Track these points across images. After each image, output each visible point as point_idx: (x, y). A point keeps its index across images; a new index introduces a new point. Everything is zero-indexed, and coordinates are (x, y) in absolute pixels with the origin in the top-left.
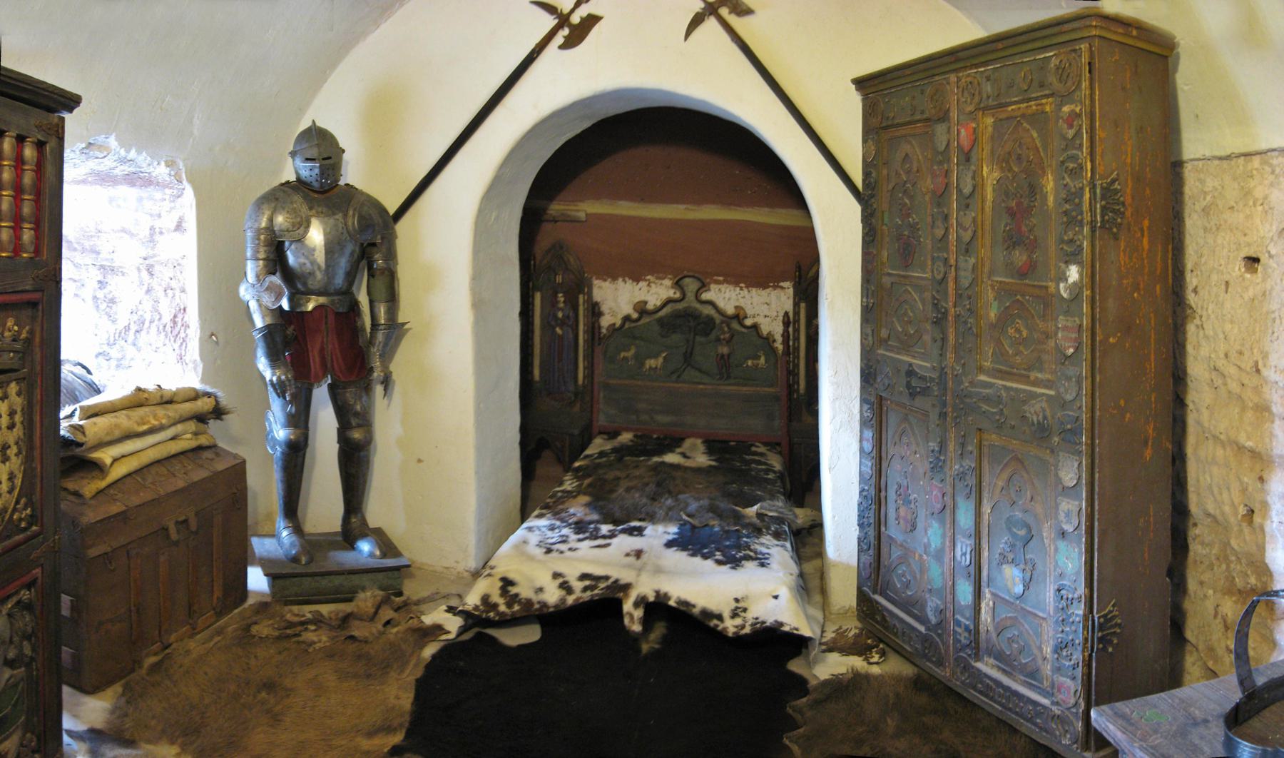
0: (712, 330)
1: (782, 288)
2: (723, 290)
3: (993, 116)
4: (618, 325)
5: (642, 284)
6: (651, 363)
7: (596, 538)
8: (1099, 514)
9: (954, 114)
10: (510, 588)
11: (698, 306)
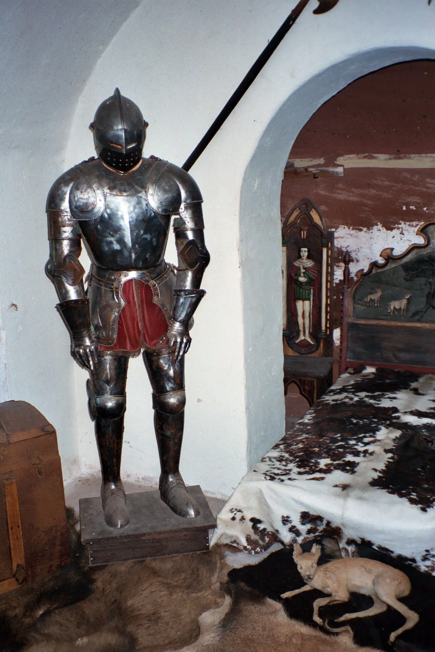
4: (365, 271)
5: (396, 232)
6: (395, 305)
7: (314, 472)
8: (314, 385)
10: (259, 525)
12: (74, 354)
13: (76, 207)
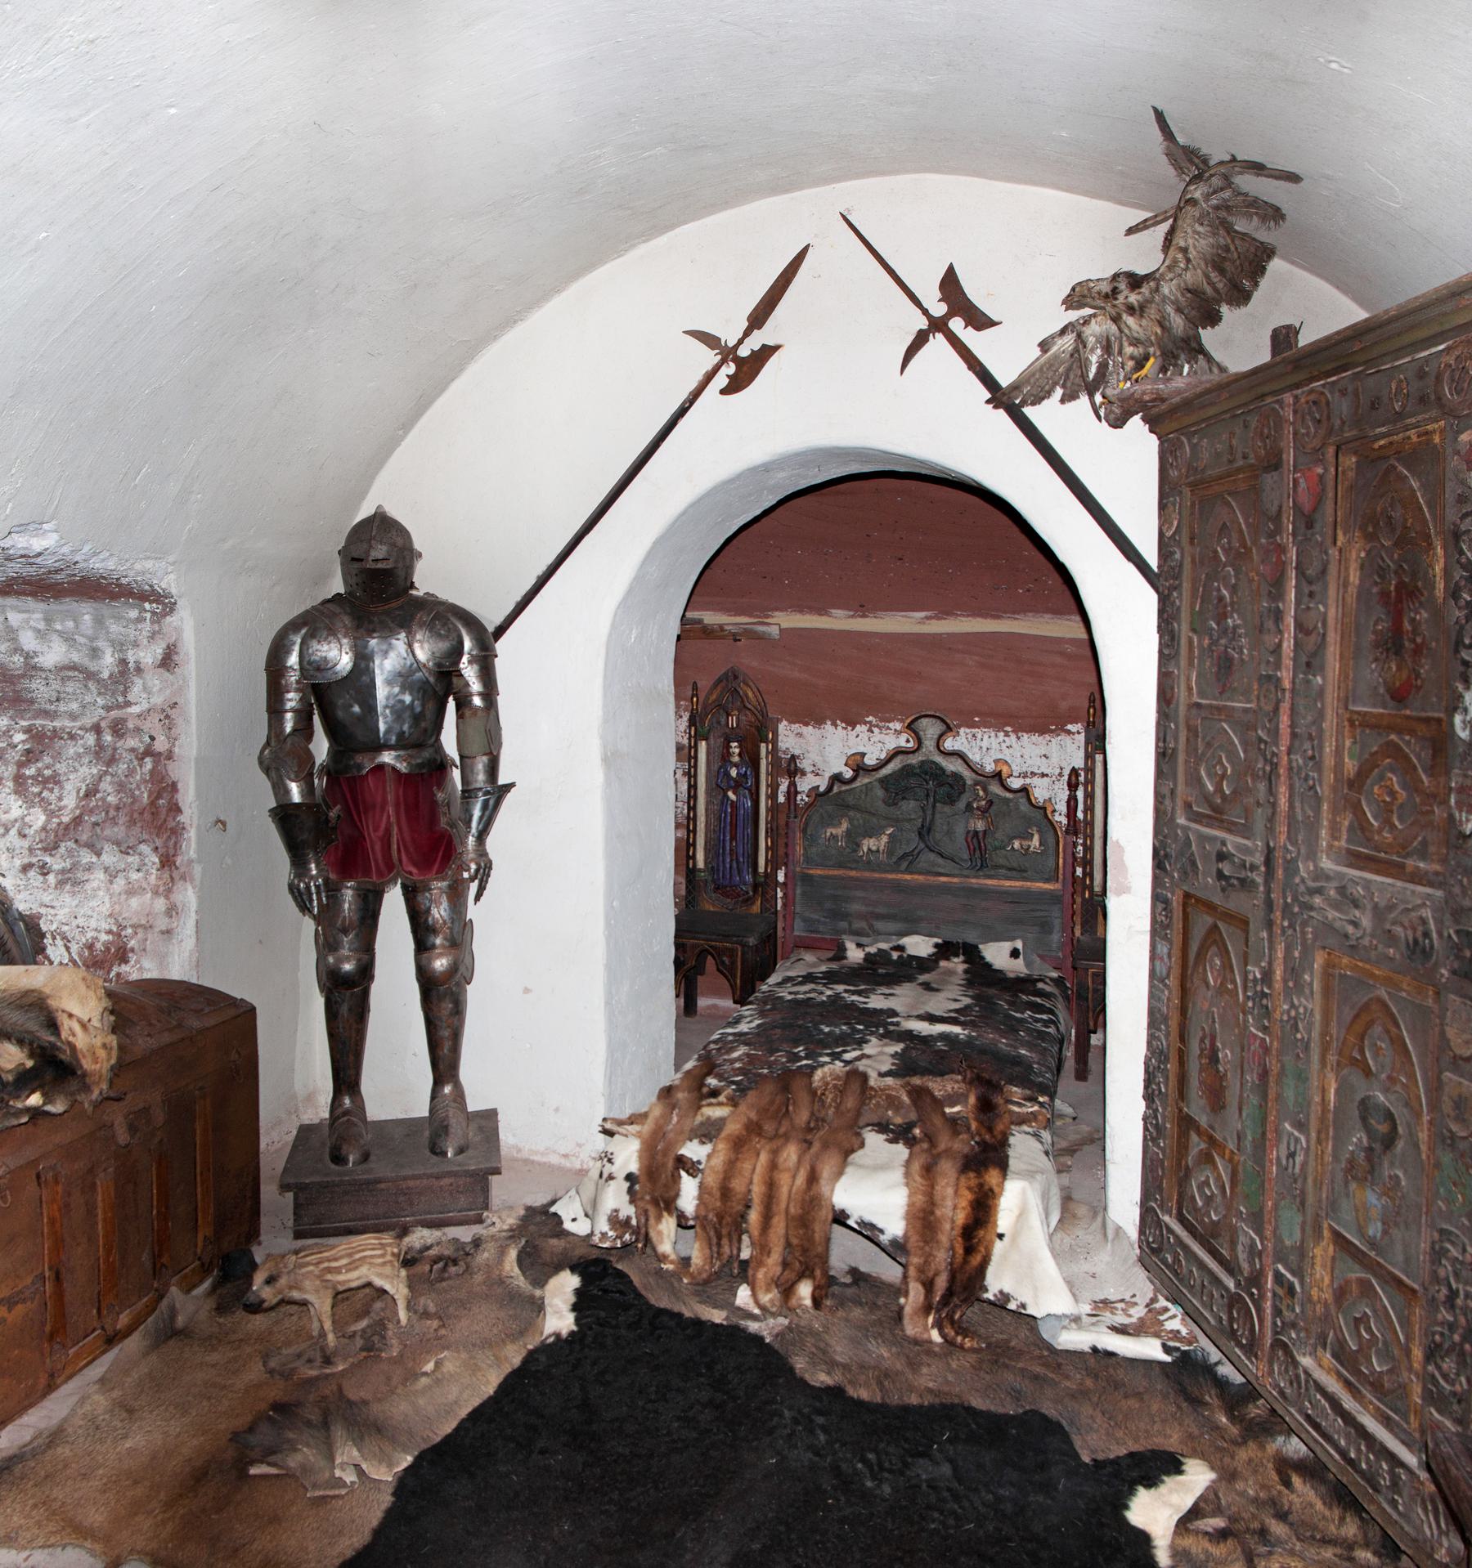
0: (961, 793)
1: (1069, 732)
2: (979, 736)
3: (1355, 453)
4: (822, 789)
9: (1289, 457)
11: (939, 759)
12: (292, 888)
13: (310, 663)
